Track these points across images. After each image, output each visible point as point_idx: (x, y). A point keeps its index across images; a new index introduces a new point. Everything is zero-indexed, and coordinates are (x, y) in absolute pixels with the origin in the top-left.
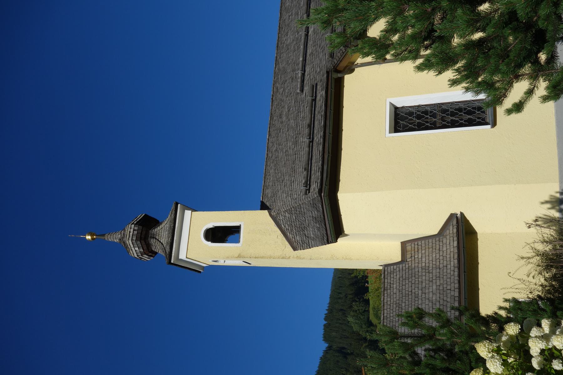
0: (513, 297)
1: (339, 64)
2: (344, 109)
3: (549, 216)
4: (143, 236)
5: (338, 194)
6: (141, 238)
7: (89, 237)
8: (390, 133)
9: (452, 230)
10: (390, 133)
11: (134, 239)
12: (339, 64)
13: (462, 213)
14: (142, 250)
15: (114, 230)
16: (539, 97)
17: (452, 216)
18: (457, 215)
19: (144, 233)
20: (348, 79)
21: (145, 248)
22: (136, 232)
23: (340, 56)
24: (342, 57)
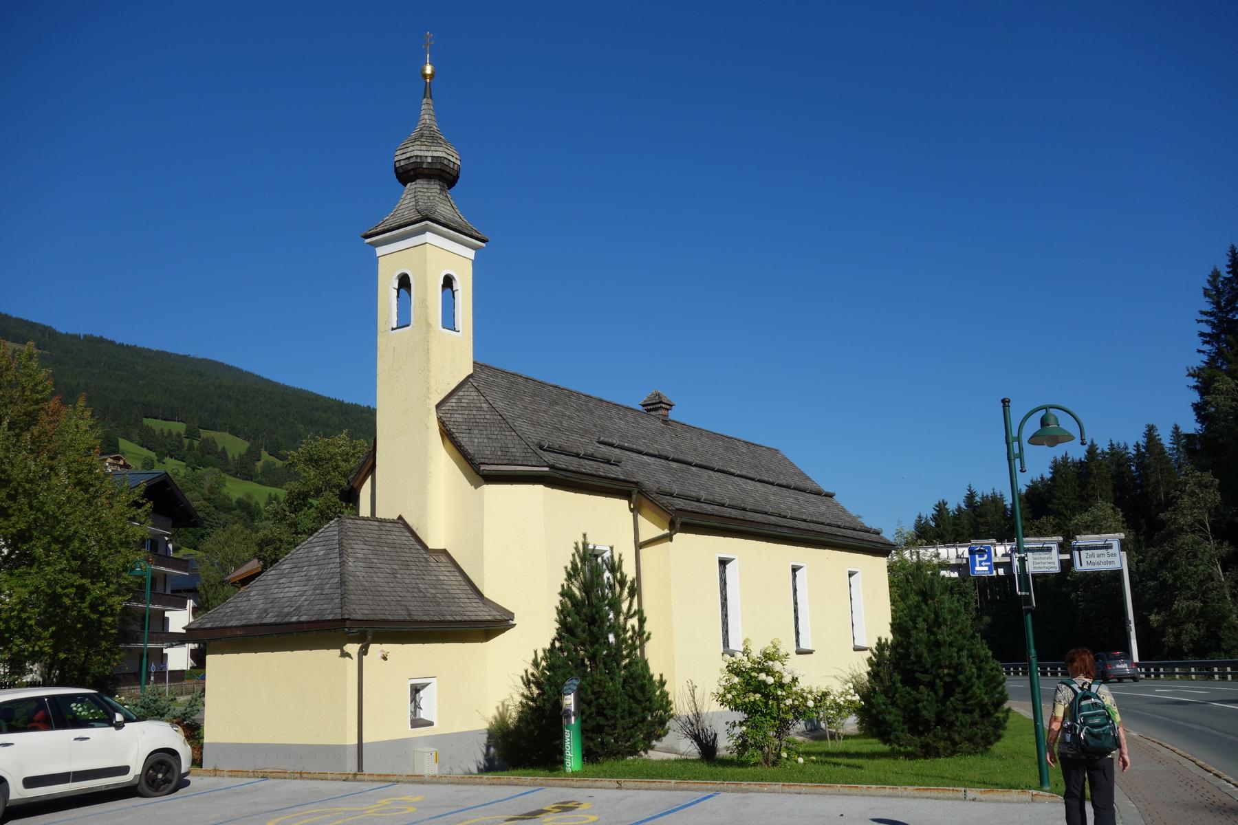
0: (647, 619)
1: (647, 498)
2: (805, 548)
3: (360, 781)
4: (444, 174)
5: (542, 486)
6: (443, 171)
7: (429, 70)
8: (719, 558)
9: (485, 615)
10: (719, 558)
11: (446, 162)
12: (647, 498)
13: (515, 625)
14: (424, 166)
15: (438, 114)
16: (661, 675)
17: (511, 616)
18: (512, 620)
19: (447, 176)
20: (623, 504)
21: (426, 171)
22: (451, 166)
23: (661, 502)
24: (660, 505)
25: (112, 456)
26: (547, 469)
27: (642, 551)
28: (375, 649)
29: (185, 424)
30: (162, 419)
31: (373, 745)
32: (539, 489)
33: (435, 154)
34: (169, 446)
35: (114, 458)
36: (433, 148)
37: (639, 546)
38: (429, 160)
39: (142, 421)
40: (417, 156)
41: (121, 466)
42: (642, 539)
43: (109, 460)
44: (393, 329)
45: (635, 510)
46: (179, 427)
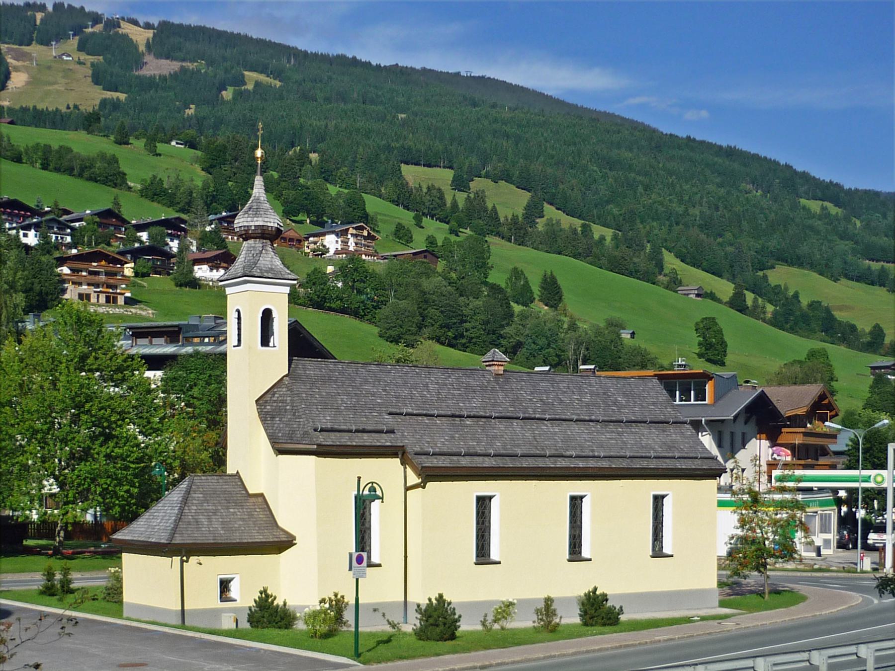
14: (250, 232)
17: (294, 538)
22: (270, 229)
25: (355, 226)
26: (315, 447)
27: (408, 492)
28: (193, 559)
29: (453, 171)
30: (424, 166)
31: (363, 605)
32: (313, 457)
33: (257, 224)
34: (427, 204)
35: (356, 228)
36: (255, 219)
37: (407, 489)
38: (253, 228)
39: (400, 170)
40: (245, 226)
41: (365, 238)
42: (408, 484)
43: (351, 231)
44: (234, 346)
45: (403, 463)
46: (443, 177)
